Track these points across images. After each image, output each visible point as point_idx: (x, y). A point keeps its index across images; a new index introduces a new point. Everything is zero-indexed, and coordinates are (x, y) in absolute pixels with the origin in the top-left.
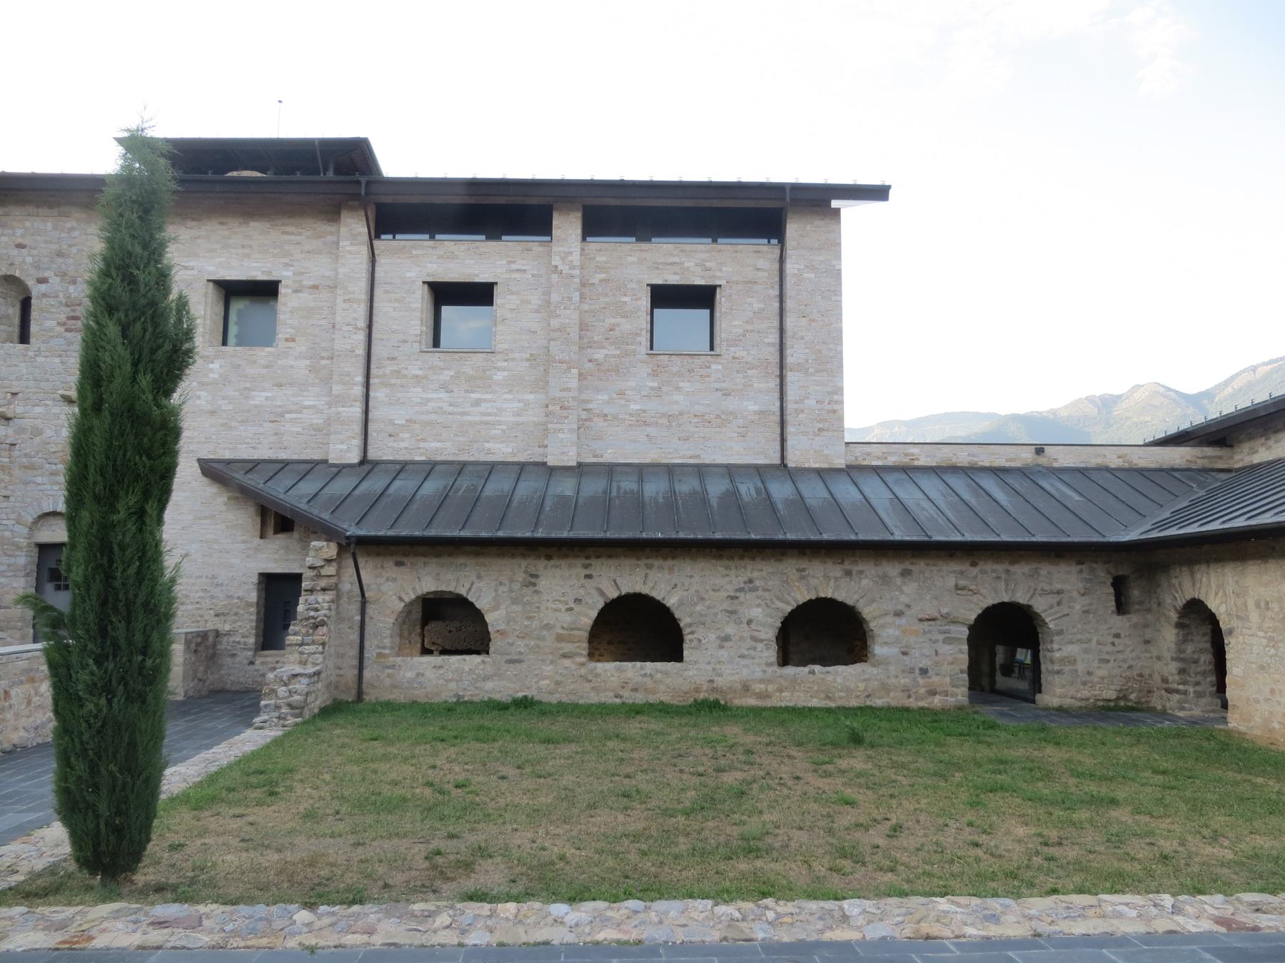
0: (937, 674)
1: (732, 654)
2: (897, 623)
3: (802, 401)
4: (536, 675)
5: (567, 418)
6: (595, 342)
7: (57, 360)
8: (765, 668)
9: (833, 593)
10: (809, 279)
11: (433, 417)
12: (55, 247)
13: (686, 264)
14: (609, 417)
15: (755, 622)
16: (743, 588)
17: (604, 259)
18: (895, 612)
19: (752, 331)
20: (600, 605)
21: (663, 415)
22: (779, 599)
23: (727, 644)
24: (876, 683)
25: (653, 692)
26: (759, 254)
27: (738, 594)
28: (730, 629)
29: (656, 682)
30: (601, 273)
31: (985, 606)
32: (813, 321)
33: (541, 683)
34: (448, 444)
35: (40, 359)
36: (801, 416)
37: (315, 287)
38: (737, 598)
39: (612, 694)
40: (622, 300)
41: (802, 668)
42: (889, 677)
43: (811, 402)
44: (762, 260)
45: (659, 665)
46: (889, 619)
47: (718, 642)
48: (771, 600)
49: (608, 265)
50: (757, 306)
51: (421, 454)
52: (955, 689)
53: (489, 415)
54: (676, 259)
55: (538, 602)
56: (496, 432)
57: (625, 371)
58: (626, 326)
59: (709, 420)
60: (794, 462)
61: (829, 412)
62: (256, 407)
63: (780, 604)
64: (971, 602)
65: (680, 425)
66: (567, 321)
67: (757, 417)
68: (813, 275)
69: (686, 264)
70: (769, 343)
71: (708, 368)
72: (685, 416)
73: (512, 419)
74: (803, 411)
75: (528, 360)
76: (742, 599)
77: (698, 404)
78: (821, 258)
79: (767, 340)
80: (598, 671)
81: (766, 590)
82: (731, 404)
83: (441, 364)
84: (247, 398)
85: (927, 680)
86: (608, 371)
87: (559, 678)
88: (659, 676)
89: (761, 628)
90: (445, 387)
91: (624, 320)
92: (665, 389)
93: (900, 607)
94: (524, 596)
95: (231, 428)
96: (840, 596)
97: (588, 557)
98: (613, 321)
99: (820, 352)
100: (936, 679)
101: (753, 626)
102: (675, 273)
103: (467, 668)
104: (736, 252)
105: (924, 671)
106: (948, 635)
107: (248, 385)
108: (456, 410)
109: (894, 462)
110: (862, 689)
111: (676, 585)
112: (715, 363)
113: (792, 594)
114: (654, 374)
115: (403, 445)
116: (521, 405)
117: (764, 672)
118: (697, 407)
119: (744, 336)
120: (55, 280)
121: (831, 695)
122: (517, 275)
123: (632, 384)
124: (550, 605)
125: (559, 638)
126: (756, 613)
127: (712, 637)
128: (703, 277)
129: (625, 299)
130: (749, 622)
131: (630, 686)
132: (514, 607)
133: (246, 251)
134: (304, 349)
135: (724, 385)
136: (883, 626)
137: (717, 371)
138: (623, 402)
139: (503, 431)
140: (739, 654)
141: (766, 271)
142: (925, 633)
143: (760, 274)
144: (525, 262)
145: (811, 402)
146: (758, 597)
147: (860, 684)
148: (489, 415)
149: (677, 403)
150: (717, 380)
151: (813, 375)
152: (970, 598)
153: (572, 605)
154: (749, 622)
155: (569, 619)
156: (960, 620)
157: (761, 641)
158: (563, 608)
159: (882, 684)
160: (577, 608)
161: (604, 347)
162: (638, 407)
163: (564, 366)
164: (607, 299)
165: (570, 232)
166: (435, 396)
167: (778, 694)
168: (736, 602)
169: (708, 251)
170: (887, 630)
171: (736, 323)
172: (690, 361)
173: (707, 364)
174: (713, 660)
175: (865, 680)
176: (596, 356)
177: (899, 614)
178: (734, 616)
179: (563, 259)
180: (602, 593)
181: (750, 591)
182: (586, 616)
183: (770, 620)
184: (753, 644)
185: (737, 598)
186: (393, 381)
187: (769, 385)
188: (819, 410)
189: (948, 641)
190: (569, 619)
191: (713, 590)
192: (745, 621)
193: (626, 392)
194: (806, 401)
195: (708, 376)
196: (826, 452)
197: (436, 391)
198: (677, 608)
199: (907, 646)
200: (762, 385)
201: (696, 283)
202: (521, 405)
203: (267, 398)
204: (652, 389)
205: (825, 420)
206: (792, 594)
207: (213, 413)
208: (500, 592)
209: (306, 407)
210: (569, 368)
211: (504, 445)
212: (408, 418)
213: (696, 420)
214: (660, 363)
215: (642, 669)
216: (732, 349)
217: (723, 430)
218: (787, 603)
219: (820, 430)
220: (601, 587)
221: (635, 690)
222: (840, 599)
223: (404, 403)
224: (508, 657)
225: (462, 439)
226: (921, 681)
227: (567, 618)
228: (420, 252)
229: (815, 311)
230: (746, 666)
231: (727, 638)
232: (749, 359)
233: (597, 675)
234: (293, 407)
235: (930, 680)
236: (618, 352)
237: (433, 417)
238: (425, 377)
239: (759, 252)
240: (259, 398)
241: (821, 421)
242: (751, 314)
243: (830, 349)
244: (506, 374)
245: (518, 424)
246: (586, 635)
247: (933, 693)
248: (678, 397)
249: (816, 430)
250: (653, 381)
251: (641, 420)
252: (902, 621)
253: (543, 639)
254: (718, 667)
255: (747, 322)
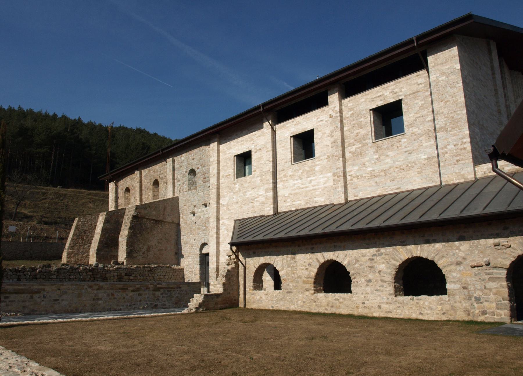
0: (486, 301)
1: (372, 289)
2: (458, 269)
3: (445, 147)
4: (297, 299)
5: (339, 181)
6: (351, 143)
7: (202, 193)
8: (389, 297)
9: (420, 254)
10: (443, 80)
11: (297, 191)
12: (200, 157)
13: (385, 94)
14: (360, 177)
15: (382, 272)
16: (376, 254)
17: (351, 104)
18: (456, 262)
19: (419, 117)
20: (318, 266)
21: (382, 171)
22: (393, 259)
23: (370, 284)
24: (448, 306)
25: (339, 307)
26: (419, 76)
27: (373, 258)
28: (371, 276)
29: (340, 303)
30: (351, 111)
31: (516, 255)
32: (447, 102)
33: (298, 302)
34: (302, 201)
35: (199, 193)
36: (446, 155)
37: (260, 149)
38: (373, 259)
39: (324, 308)
40: (360, 120)
41: (407, 297)
42: (455, 302)
43: (451, 147)
44: (420, 79)
45: (341, 295)
46: (453, 267)
47: (366, 283)
48: (389, 260)
49: (353, 107)
50: (420, 103)
51: (294, 207)
52: (499, 311)
53: (315, 186)
54: (381, 94)
55: (296, 266)
56: (318, 193)
57: (364, 153)
58: (363, 132)
59: (403, 168)
60: (445, 182)
61: (461, 149)
62: (247, 198)
63: (393, 262)
64: (506, 253)
65: (390, 174)
66: (337, 137)
67: (427, 161)
68: (444, 77)
69: (385, 94)
70: (428, 121)
71: (400, 142)
72: (392, 169)
73: (323, 186)
74: (446, 153)
75: (327, 158)
76: (375, 260)
77: (398, 161)
78: (447, 67)
79: (427, 120)
80: (318, 297)
81: (386, 254)
82: (413, 158)
83: (298, 168)
84: (245, 195)
85: (480, 304)
86: (357, 155)
87: (304, 300)
88: (341, 300)
89: (385, 275)
90: (300, 178)
91: (361, 130)
92: (381, 158)
93: (459, 259)
94: (291, 264)
95: (242, 207)
96: (424, 255)
97: (312, 244)
98: (357, 131)
99: (453, 117)
100: (486, 304)
101: (382, 274)
102: (381, 100)
103: (274, 295)
104: (408, 79)
105: (478, 299)
106: (491, 276)
107: (245, 191)
108: (304, 186)
109: (508, 170)
110: (440, 309)
111: (346, 255)
112: (403, 138)
113: (399, 256)
114: (376, 152)
115: (288, 204)
116: (326, 179)
117: (388, 298)
118: (397, 163)
119: (416, 120)
120: (200, 167)
121: (422, 312)
122: (320, 123)
123: (367, 159)
124: (300, 267)
125: (304, 282)
126: (382, 267)
127: (363, 280)
128: (393, 98)
129: (361, 120)
130: (380, 272)
131: (330, 305)
132: (288, 268)
133: (242, 142)
134: (258, 173)
135: (408, 149)
136: (450, 272)
137: (404, 142)
138: (364, 168)
139: (320, 192)
140: (376, 289)
141: (423, 84)
142: (476, 275)
143: (420, 86)
144: (322, 116)
145: (451, 147)
146: (383, 258)
147: (438, 306)
148: (315, 186)
149: (388, 163)
150: (406, 147)
151: (450, 131)
152: (504, 251)
153: (308, 267)
154: (380, 272)
155: (307, 273)
156: (499, 266)
157: (386, 282)
158: (304, 268)
159: (452, 306)
160: (310, 268)
161: (354, 145)
162: (371, 169)
163: (337, 158)
164: (354, 122)
165: (335, 97)
166: (297, 182)
167: (395, 311)
168: (373, 261)
169: (394, 84)
170: (452, 274)
171: (412, 115)
172: (392, 140)
173: (399, 140)
174: (364, 292)
175: (441, 304)
176: (352, 150)
177: (459, 264)
178: (372, 269)
179: (333, 110)
180: (318, 261)
181: (379, 255)
182: (313, 271)
183: (389, 271)
184: (382, 283)
185: (373, 259)
186: (284, 179)
187: (431, 143)
188: (456, 150)
189: (493, 279)
190: (307, 273)
191: (362, 256)
192: (377, 271)
193: (366, 163)
194: (448, 147)
195: (400, 146)
196: (462, 173)
197: (297, 180)
198: (347, 266)
199: (465, 283)
200: (428, 144)
201: (391, 102)
202: (326, 179)
203: (250, 194)
204: (376, 159)
205: (460, 155)
206: (399, 256)
207: (237, 203)
208: (284, 262)
209: (260, 195)
210: (339, 158)
211: (321, 198)
212: (289, 193)
213: (397, 170)
214: (378, 145)
215: (334, 296)
216: (410, 129)
217: (410, 172)
218: (397, 260)
219: (458, 161)
220: (318, 258)
221: (332, 307)
222: (424, 257)
223: (287, 187)
224: (287, 291)
225: (306, 198)
226: (476, 305)
227: (306, 273)
228: (288, 125)
229: (447, 96)
230: (379, 295)
231: (369, 281)
232: (420, 132)
233: (318, 299)
234: (257, 196)
235: (482, 305)
236: (360, 145)
237: (297, 191)
238: (293, 175)
239: (419, 75)
240: (248, 195)
241: (458, 156)
242: (418, 108)
243: (458, 114)
244: (319, 167)
245: (325, 188)
246: (313, 280)
247: (484, 313)
248: (388, 160)
249: (455, 161)
250: (376, 155)
251: (373, 175)
252: (462, 268)
253: (298, 282)
254: (366, 295)
255: (417, 113)
